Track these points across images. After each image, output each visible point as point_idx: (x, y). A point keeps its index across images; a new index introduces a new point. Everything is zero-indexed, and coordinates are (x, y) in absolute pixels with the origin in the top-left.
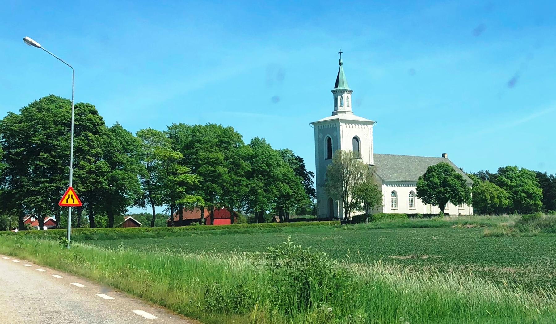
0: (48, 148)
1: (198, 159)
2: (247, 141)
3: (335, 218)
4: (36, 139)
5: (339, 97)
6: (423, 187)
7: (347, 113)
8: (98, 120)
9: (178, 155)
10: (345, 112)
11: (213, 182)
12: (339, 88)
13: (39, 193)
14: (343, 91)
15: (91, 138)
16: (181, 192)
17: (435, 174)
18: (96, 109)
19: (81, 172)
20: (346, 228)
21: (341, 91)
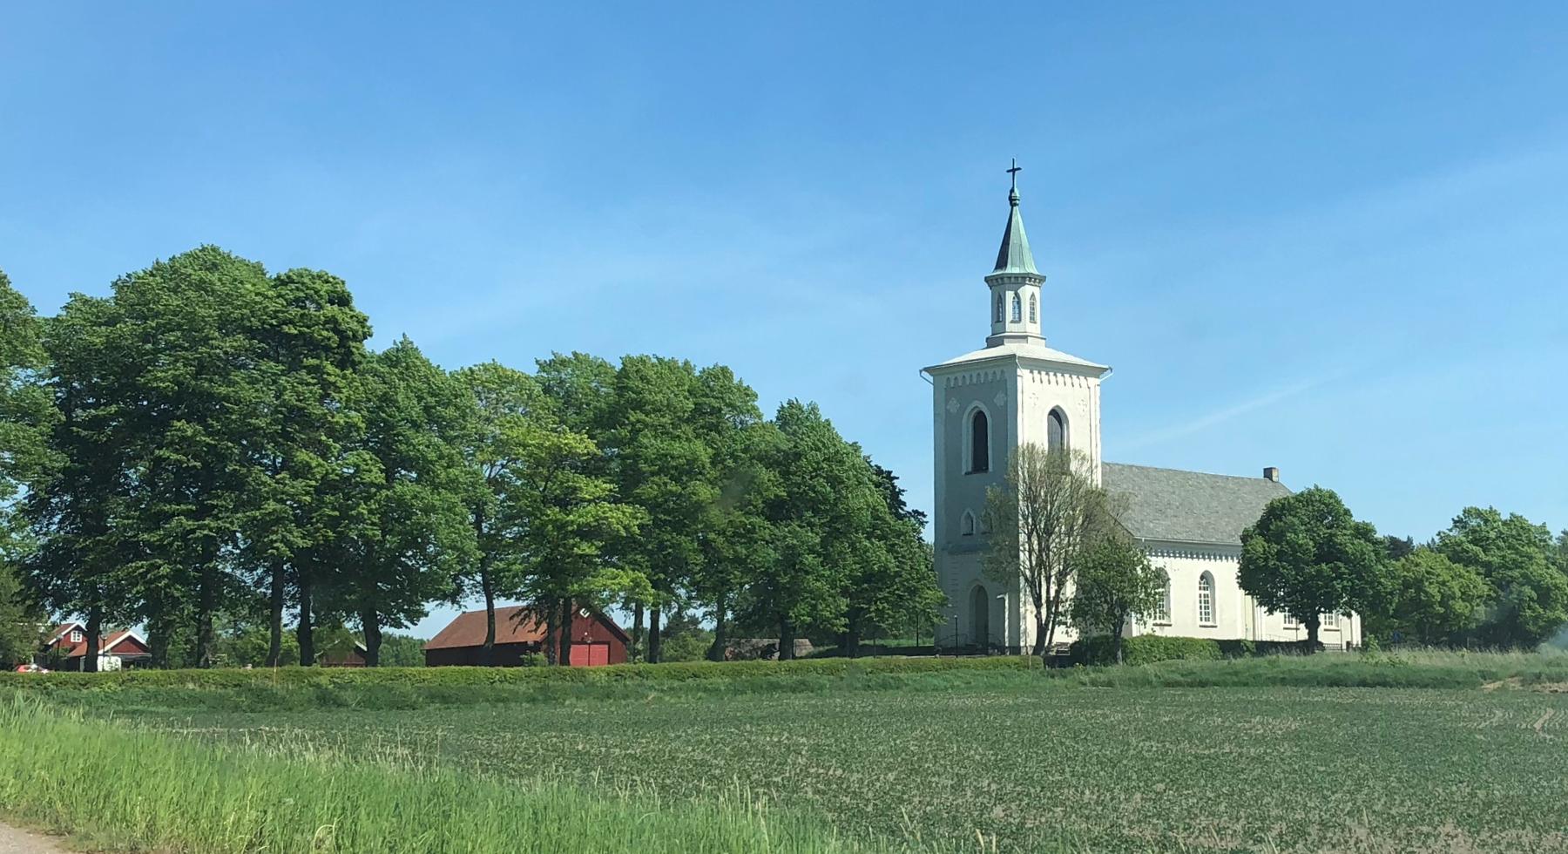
0: (197, 405)
2: (769, 412)
3: (994, 646)
4: (165, 374)
5: (1010, 295)
6: (1266, 560)
8: (355, 325)
9: (582, 444)
10: (1025, 337)
11: (679, 527)
12: (1011, 269)
13: (161, 550)
14: (1023, 279)
15: (332, 379)
17: (1296, 521)
18: (348, 288)
19: (300, 484)
20: (1085, 679)
21: (1016, 276)
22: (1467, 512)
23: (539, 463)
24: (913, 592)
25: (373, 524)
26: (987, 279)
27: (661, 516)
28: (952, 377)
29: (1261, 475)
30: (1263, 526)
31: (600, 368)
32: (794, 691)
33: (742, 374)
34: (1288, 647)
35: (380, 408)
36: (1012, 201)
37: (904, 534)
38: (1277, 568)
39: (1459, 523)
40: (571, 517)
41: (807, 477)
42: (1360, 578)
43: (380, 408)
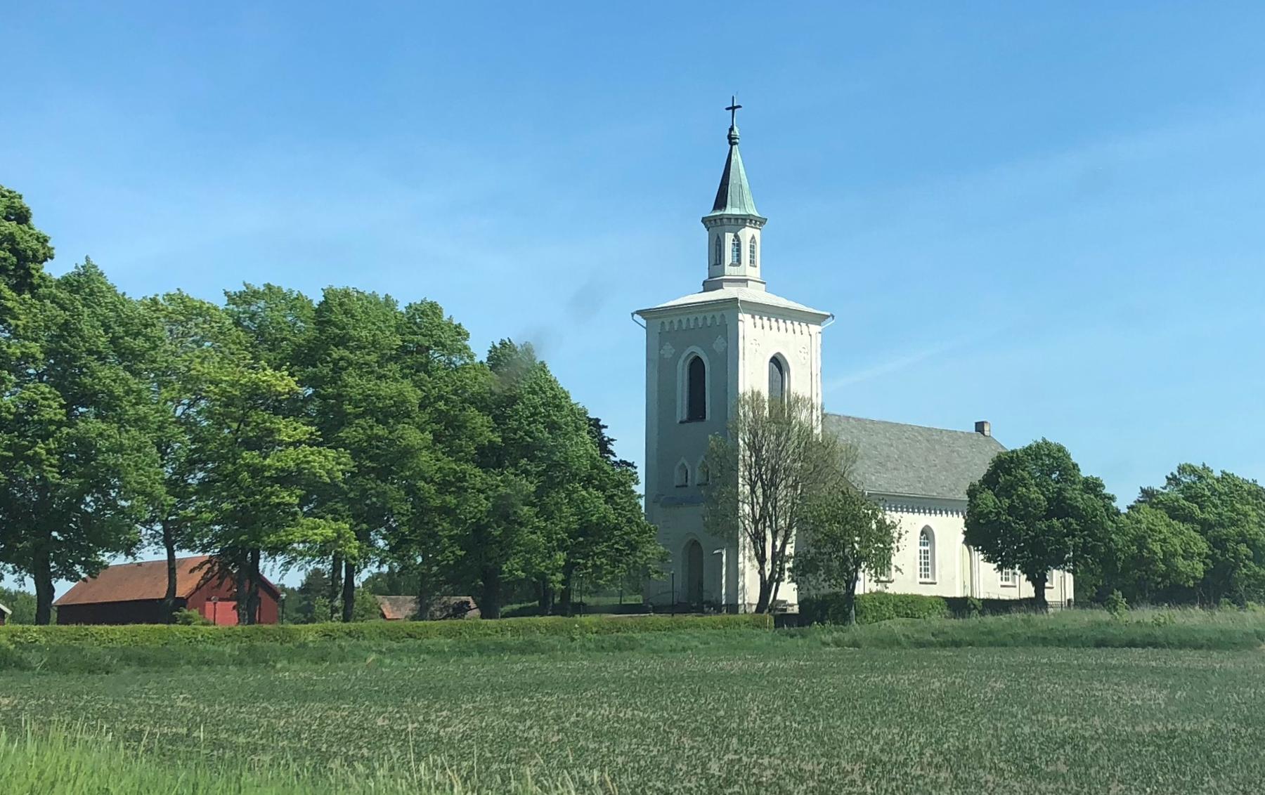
1: (339, 397)
5: (729, 237)
6: (998, 514)
7: (750, 282)
9: (284, 382)
11: (384, 474)
12: (729, 210)
14: (743, 221)
15: (9, 304)
18: (26, 202)
20: (828, 638)
22: (1182, 469)
23: (230, 402)
24: (633, 547)
25: (51, 465)
26: (704, 220)
27: (368, 464)
29: (973, 429)
30: (990, 480)
31: (295, 303)
33: (452, 312)
34: (1019, 603)
35: (61, 337)
36: (732, 140)
37: (624, 484)
39: (1172, 480)
40: (268, 461)
41: (518, 419)
42: (1092, 535)
43: (61, 337)
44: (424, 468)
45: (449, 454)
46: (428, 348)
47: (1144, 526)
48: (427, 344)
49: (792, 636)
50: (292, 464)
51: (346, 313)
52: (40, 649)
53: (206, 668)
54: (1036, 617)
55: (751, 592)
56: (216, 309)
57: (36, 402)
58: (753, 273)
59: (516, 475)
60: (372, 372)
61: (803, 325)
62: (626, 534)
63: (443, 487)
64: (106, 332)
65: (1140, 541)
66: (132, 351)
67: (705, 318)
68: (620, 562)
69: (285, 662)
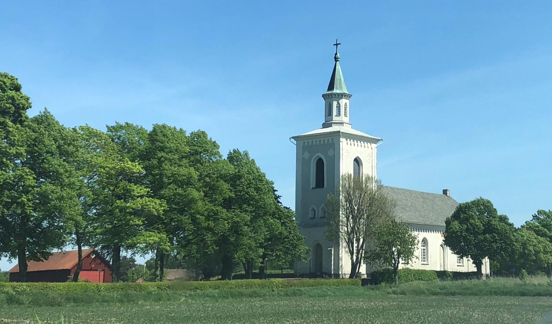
3: (326, 274)
5: (335, 103)
7: (344, 123)
9: (137, 168)
11: (181, 212)
12: (336, 91)
14: (342, 96)
15: (11, 129)
16: (138, 225)
18: (19, 82)
20: (390, 290)
22: (539, 212)
26: (324, 96)
27: (174, 206)
28: (314, 140)
30: (456, 216)
31: (140, 131)
32: (251, 296)
33: (212, 135)
36: (336, 59)
37: (289, 217)
38: (466, 236)
39: (535, 217)
40: (128, 205)
41: (242, 185)
44: (200, 209)
45: (211, 202)
46: (201, 153)
47: (525, 238)
48: (200, 150)
49: (372, 289)
50: (140, 205)
51: (164, 135)
52: (28, 294)
53: (106, 304)
54: (475, 281)
55: (346, 267)
56: (103, 133)
57: (23, 176)
58: (346, 120)
59: (241, 212)
60: (175, 163)
61: (369, 144)
62: (291, 240)
63: (208, 218)
64: (55, 142)
65: (524, 245)
66: (67, 152)
67: (324, 140)
68: (288, 254)
69: (143, 301)
